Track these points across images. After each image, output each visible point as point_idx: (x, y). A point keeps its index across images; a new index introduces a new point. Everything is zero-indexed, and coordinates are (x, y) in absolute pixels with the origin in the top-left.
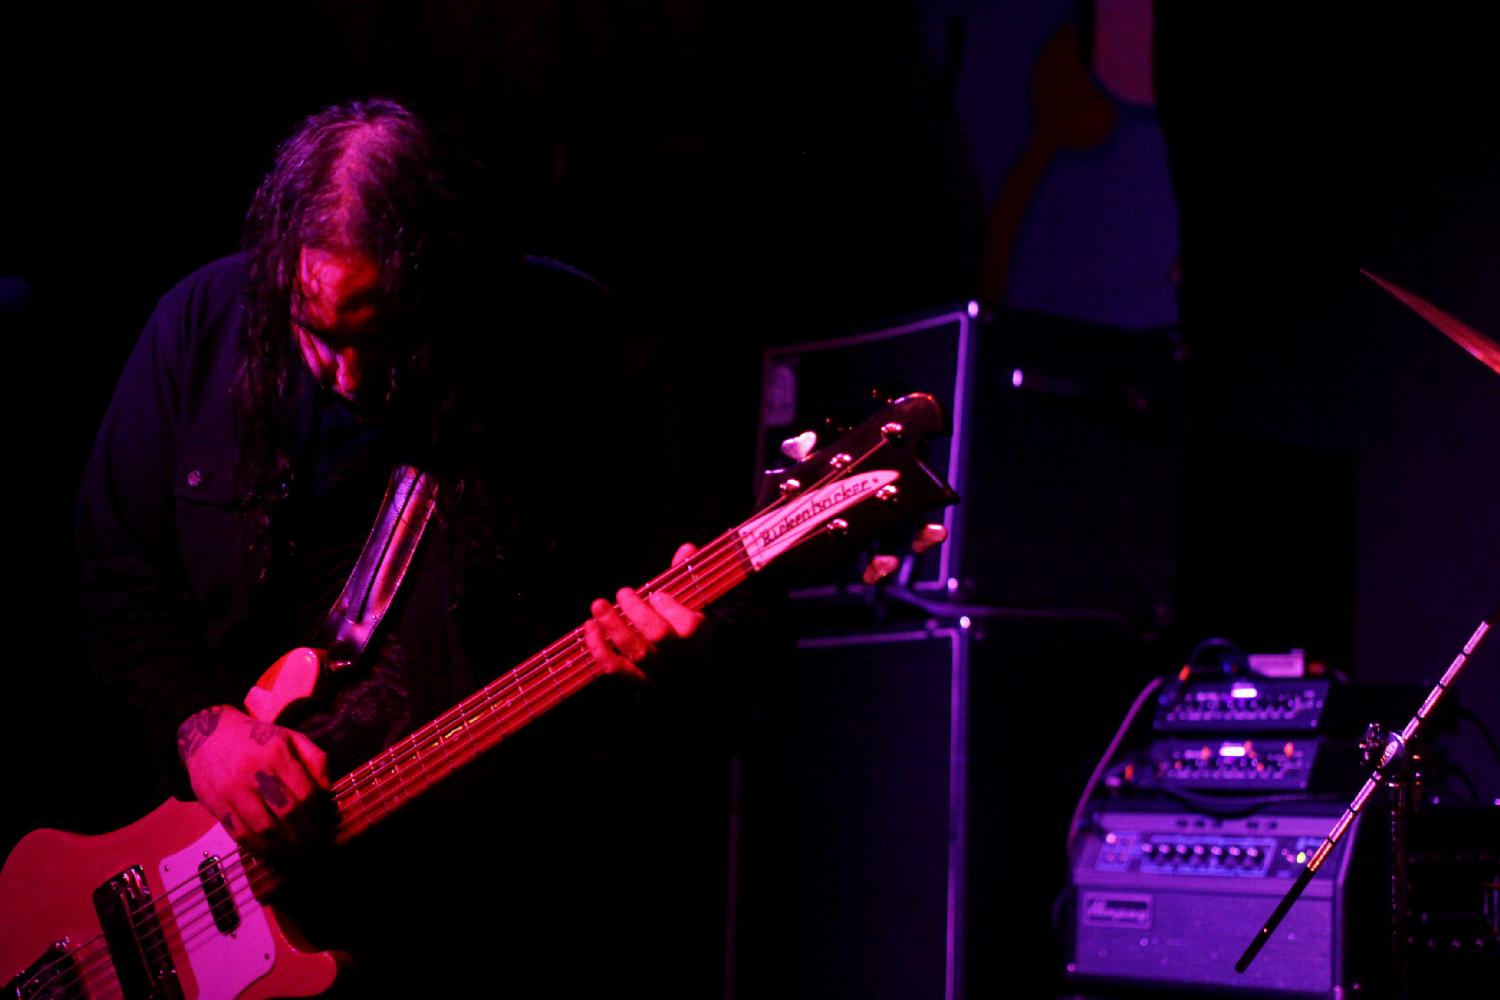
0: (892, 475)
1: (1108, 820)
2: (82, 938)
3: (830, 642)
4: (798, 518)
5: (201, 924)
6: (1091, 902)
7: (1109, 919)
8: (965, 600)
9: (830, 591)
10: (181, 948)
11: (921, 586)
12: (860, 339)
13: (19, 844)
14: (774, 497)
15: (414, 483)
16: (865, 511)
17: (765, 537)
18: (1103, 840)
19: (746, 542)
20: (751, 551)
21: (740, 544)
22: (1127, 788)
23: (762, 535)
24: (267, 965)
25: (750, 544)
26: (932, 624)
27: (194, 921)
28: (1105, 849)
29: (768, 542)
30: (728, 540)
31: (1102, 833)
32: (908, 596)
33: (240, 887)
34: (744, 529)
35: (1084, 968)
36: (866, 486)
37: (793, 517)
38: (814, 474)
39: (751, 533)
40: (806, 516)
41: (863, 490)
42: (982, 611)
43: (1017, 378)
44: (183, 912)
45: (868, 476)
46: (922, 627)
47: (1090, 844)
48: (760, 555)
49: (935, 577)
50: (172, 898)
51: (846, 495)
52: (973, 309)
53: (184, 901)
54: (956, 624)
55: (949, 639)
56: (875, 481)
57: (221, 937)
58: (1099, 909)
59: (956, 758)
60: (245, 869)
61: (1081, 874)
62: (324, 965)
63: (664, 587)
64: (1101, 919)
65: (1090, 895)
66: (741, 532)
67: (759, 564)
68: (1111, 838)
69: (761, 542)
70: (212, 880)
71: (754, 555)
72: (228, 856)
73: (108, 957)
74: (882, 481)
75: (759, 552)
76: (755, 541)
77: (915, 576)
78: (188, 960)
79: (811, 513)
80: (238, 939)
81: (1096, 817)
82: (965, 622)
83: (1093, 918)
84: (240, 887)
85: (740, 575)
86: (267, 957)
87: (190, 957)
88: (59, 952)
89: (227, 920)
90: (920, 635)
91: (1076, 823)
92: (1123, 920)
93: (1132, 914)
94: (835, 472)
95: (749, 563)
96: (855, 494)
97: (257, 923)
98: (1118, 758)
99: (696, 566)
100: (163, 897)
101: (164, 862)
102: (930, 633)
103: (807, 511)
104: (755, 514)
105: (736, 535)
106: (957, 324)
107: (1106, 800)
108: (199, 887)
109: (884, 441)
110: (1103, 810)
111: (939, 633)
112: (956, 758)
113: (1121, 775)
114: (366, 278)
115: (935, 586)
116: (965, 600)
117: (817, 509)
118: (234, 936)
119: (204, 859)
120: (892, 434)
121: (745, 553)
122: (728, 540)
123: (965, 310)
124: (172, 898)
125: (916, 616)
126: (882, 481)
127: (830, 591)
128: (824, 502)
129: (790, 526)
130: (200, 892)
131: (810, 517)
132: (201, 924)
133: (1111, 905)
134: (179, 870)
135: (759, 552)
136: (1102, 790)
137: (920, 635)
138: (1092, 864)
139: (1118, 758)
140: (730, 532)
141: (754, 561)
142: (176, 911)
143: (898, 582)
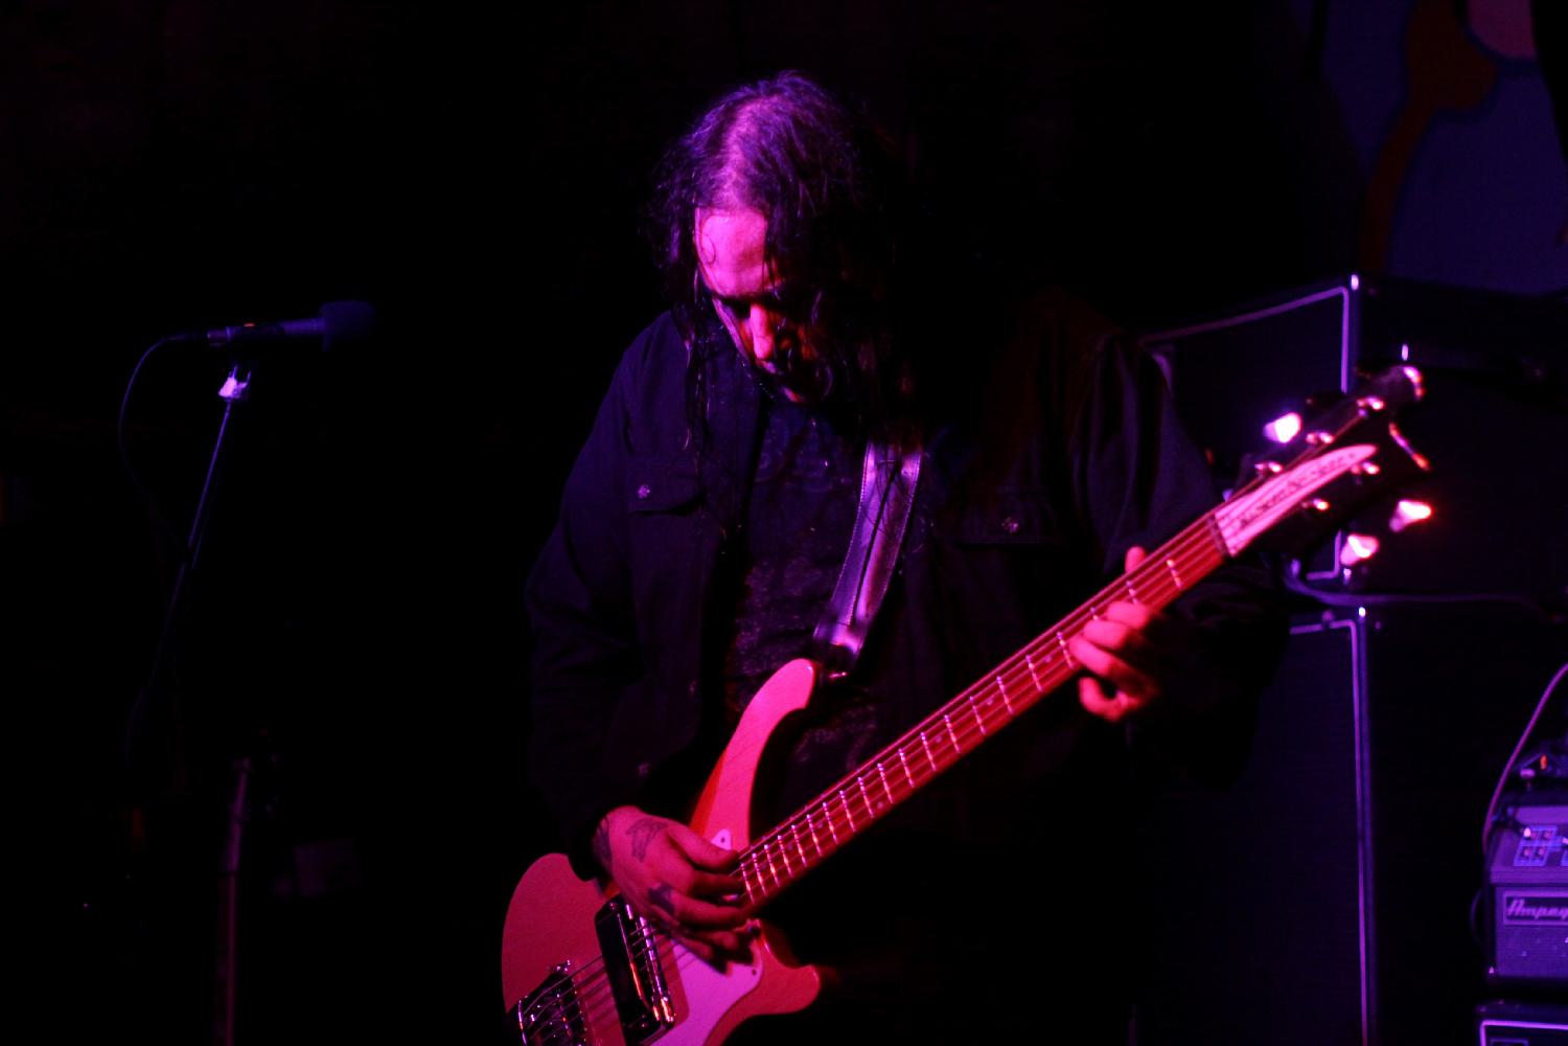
0: (1365, 451)
1: (1523, 814)
6: (1510, 900)
7: (1530, 918)
11: (1313, 576)
12: (1239, 320)
14: (1249, 482)
16: (1341, 488)
17: (1241, 521)
18: (1521, 835)
19: (1222, 524)
20: (1226, 533)
21: (1216, 527)
22: (1541, 779)
23: (1238, 517)
26: (1327, 616)
28: (1522, 843)
29: (1245, 524)
31: (1518, 828)
32: (1302, 589)
34: (1219, 514)
35: (1503, 971)
37: (1270, 496)
38: (1290, 456)
39: (1227, 515)
40: (1282, 496)
41: (1340, 466)
42: (1381, 599)
46: (1318, 620)
47: (1505, 841)
52: (1355, 282)
55: (1348, 629)
58: (1517, 907)
61: (1498, 872)
64: (1520, 917)
65: (1506, 895)
67: (1235, 548)
68: (1527, 833)
69: (1237, 524)
71: (1229, 537)
73: (605, 976)
74: (1356, 457)
75: (1235, 534)
76: (1232, 521)
78: (679, 976)
79: (1287, 492)
81: (1510, 811)
82: (1362, 612)
83: (1512, 917)
85: (1216, 559)
87: (681, 974)
88: (560, 975)
90: (1317, 628)
91: (1490, 819)
92: (1542, 918)
93: (1553, 912)
95: (1224, 546)
96: (1333, 470)
98: (1531, 747)
102: (1326, 625)
103: (1282, 492)
105: (1213, 517)
106: (1340, 296)
107: (1519, 793)
110: (1517, 805)
111: (1335, 625)
112: (1361, 756)
113: (1535, 766)
114: (237, 397)
115: (1329, 575)
117: (1293, 489)
121: (1220, 536)
123: (1348, 284)
125: (1313, 608)
126: (1356, 457)
129: (1265, 507)
131: (1286, 497)
133: (1529, 902)
135: (1235, 534)
136: (1515, 781)
137: (1317, 628)
138: (1508, 862)
139: (1531, 747)
140: (1207, 515)
141: (1230, 543)
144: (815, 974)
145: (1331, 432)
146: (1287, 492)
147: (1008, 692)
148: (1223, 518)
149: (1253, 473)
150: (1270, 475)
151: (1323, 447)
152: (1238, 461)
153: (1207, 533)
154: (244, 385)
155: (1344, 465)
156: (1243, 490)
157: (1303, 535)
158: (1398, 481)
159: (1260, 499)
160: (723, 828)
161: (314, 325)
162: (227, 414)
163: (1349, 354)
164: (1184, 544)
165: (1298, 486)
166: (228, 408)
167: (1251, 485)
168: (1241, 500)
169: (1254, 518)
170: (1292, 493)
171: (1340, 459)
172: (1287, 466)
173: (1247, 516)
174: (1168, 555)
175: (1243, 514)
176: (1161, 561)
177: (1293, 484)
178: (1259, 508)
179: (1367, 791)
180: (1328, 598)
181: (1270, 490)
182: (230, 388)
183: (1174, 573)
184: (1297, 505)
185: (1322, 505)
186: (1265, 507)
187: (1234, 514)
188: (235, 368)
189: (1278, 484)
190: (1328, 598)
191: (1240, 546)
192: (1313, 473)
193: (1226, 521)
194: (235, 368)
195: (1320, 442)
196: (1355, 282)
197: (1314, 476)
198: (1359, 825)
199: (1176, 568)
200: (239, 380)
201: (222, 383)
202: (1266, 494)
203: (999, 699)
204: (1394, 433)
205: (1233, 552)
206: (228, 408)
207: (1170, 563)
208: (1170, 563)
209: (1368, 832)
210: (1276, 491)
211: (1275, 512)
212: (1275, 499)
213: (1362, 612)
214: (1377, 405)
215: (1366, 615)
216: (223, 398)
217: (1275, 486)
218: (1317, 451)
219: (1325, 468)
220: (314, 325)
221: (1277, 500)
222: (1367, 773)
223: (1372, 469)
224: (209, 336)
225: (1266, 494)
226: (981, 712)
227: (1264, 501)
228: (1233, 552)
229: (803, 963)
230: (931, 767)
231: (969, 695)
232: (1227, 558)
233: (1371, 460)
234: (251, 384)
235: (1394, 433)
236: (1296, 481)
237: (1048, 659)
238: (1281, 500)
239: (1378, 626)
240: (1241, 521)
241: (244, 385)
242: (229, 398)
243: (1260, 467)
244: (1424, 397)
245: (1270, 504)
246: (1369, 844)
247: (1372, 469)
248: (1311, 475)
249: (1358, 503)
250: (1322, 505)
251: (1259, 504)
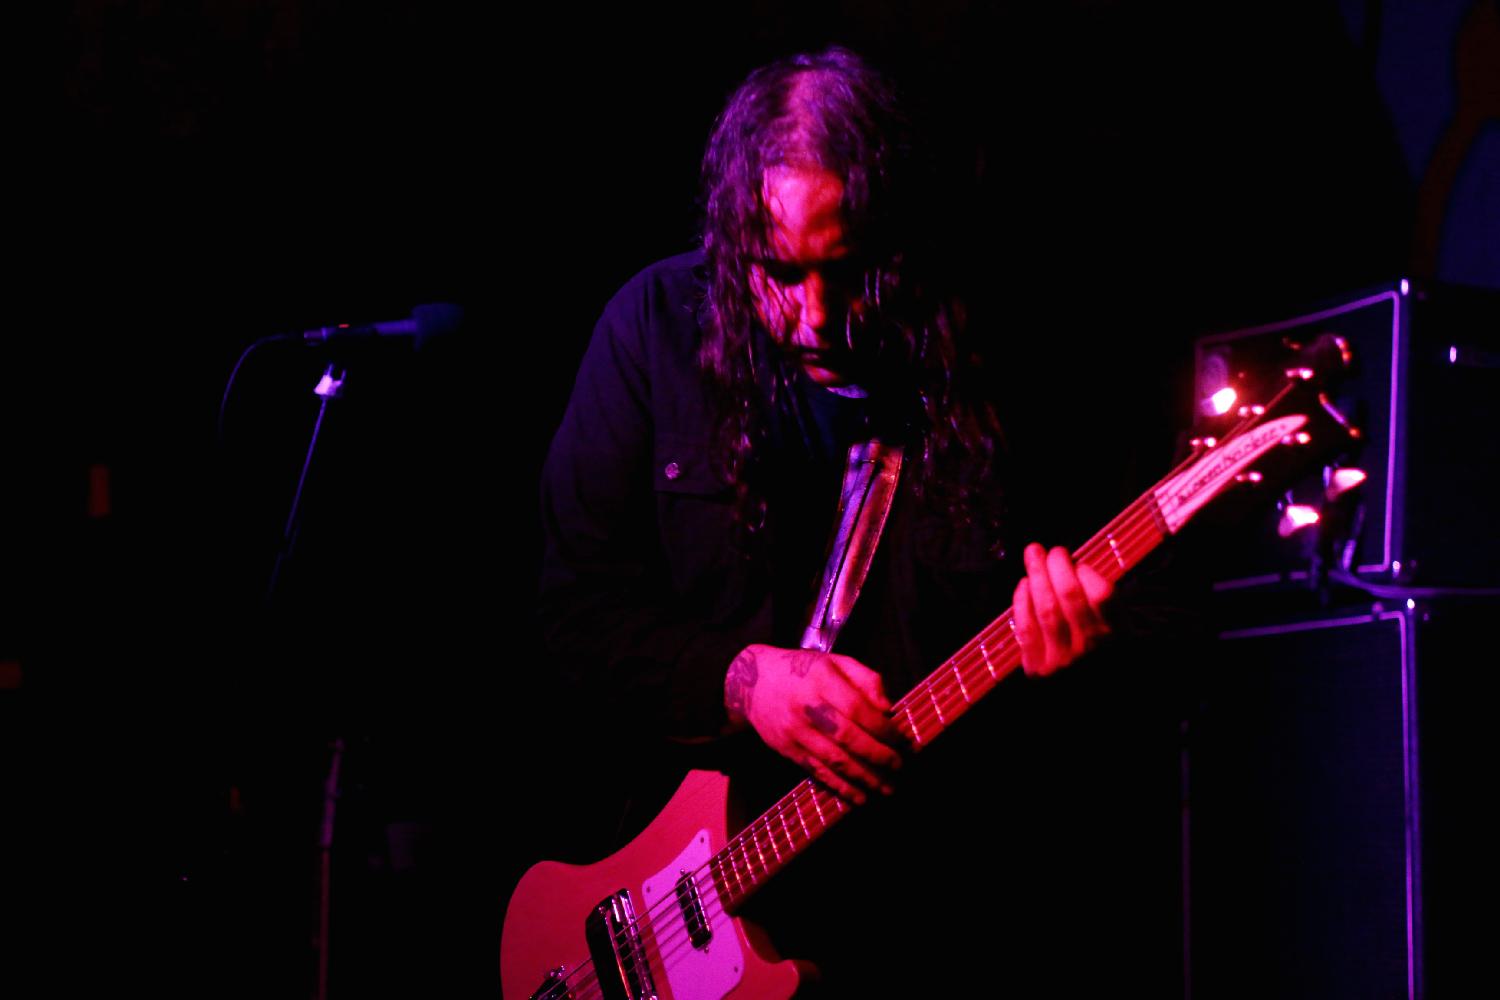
0: (1297, 421)
2: (575, 967)
3: (1276, 630)
4: (1210, 474)
5: (677, 940)
8: (1410, 580)
9: (1275, 578)
10: (661, 966)
11: (1364, 569)
13: (516, 892)
15: (867, 492)
16: (1275, 460)
17: (1179, 498)
19: (1161, 502)
20: (1166, 511)
21: (1156, 504)
23: (1176, 494)
24: (736, 978)
25: (1169, 514)
26: (1377, 608)
27: (672, 937)
29: (1183, 500)
30: (1144, 502)
32: (1353, 581)
33: (710, 903)
34: (1157, 493)
36: (1275, 433)
37: (1205, 472)
38: (1226, 428)
39: (1166, 492)
41: (1272, 438)
42: (1427, 592)
43: (1453, 355)
44: (663, 929)
45: (1275, 425)
46: (1369, 611)
48: (1175, 516)
49: (1380, 561)
50: (652, 915)
51: (1255, 446)
52: (1405, 287)
53: (660, 921)
54: (1403, 607)
55: (1397, 620)
56: (1283, 427)
57: (694, 951)
59: (1408, 742)
60: (719, 893)
62: (790, 971)
63: (1085, 557)
66: (1157, 493)
67: (1174, 524)
69: (1176, 501)
70: (684, 891)
72: (700, 870)
74: (1288, 428)
75: (1174, 511)
76: (1170, 499)
77: (1357, 560)
79: (1223, 467)
80: (710, 953)
82: (1411, 604)
84: (710, 903)
85: (1156, 539)
86: (736, 970)
89: (701, 938)
90: (1367, 619)
94: (1242, 422)
95: (1164, 523)
97: (726, 932)
99: (1122, 540)
100: (644, 916)
101: (645, 885)
102: (1376, 616)
103: (1218, 466)
104: (1173, 469)
105: (1152, 496)
106: (1391, 301)
108: (675, 903)
109: (1290, 386)
111: (1385, 617)
112: (1408, 742)
115: (1379, 568)
116: (1410, 580)
117: (1228, 463)
118: (707, 952)
119: (680, 876)
120: (1299, 379)
121: (1160, 514)
122: (1144, 502)
123: (1398, 289)
124: (652, 915)
125: (1363, 601)
126: (1288, 428)
127: (1275, 578)
128: (1235, 454)
129: (1202, 483)
130: (675, 908)
131: (1222, 471)
132: (677, 940)
134: (660, 886)
135: (1174, 511)
137: (1367, 619)
141: (1170, 520)
142: (655, 929)
143: (1342, 566)
144: (794, 969)
145: (1262, 403)
146: (1223, 467)
147: (964, 681)
148: (1161, 496)
149: (1190, 449)
150: (1205, 451)
151: (1255, 420)
152: (1175, 436)
153: (1148, 511)
154: (338, 383)
155: (1276, 436)
156: (1179, 467)
157: (1242, 510)
158: (1330, 448)
159: (1196, 475)
160: (702, 828)
161: (406, 326)
162: (322, 412)
163: (1400, 350)
164: (1127, 522)
165: (1233, 460)
166: (324, 405)
167: (1188, 461)
168: (1177, 477)
169: (1190, 496)
170: (1226, 468)
171: (1272, 431)
172: (1221, 442)
173: (1184, 493)
174: (1109, 536)
175: (1180, 490)
176: (1104, 541)
177: (1229, 458)
178: (1196, 484)
179: (1415, 778)
180: (1377, 590)
181: (1206, 466)
182: (325, 385)
183: (1117, 553)
184: (1233, 479)
185: (1255, 477)
186: (1202, 483)
187: (1172, 491)
188: (330, 367)
189: (1215, 458)
190: (1377, 590)
191: (1179, 524)
192: (1248, 446)
193: (1166, 498)
194: (330, 367)
195: (1252, 415)
196: (1405, 287)
197: (1249, 449)
198: (1407, 809)
199: (1119, 548)
200: (335, 378)
201: (318, 381)
202: (1202, 469)
203: (957, 687)
204: (1323, 401)
205: (1172, 529)
206: (324, 405)
207: (1112, 543)
208: (1112, 543)
209: (1416, 815)
210: (1211, 467)
211: (1215, 484)
212: (1212, 474)
213: (1411, 604)
214: (1306, 374)
215: (1414, 609)
216: (319, 396)
217: (1211, 461)
218: (1251, 423)
219: (1258, 440)
220: (406, 326)
221: (1213, 475)
222: (1415, 758)
223: (1303, 438)
224: (305, 336)
225: (1202, 469)
226: (939, 702)
227: (1201, 476)
228: (1172, 529)
229: (784, 957)
230: (803, 833)
231: (928, 684)
232: (1167, 535)
233: (1301, 430)
234: (345, 382)
235: (1323, 401)
236: (1232, 456)
237: (1000, 645)
238: (1217, 475)
239: (1426, 617)
240: (1179, 498)
241: (338, 383)
242: (325, 395)
243: (1195, 442)
244: (1353, 359)
245: (1206, 480)
246: (1416, 827)
247: (1303, 438)
248: (1244, 447)
249: (1287, 472)
250: (1255, 477)
251: (1196, 480)
